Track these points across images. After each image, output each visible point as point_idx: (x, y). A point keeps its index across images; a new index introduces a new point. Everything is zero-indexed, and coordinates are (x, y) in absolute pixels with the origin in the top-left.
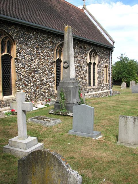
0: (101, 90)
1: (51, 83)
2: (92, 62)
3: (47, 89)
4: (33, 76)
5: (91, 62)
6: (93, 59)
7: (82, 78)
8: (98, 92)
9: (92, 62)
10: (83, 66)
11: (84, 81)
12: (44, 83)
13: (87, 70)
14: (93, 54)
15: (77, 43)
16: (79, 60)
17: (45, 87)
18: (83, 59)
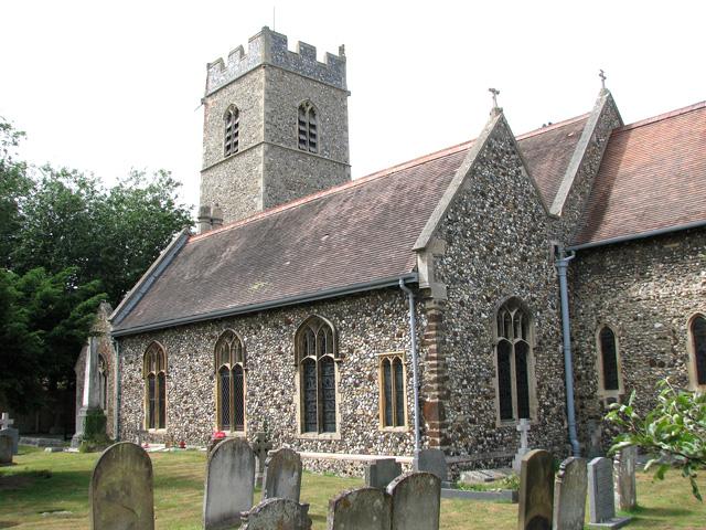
0: (361, 452)
1: (209, 414)
2: (513, 341)
4: (186, 402)
6: (516, 330)
7: (279, 407)
8: (340, 456)
9: (513, 341)
14: (513, 314)
15: (263, 318)
17: (201, 421)
18: (281, 353)
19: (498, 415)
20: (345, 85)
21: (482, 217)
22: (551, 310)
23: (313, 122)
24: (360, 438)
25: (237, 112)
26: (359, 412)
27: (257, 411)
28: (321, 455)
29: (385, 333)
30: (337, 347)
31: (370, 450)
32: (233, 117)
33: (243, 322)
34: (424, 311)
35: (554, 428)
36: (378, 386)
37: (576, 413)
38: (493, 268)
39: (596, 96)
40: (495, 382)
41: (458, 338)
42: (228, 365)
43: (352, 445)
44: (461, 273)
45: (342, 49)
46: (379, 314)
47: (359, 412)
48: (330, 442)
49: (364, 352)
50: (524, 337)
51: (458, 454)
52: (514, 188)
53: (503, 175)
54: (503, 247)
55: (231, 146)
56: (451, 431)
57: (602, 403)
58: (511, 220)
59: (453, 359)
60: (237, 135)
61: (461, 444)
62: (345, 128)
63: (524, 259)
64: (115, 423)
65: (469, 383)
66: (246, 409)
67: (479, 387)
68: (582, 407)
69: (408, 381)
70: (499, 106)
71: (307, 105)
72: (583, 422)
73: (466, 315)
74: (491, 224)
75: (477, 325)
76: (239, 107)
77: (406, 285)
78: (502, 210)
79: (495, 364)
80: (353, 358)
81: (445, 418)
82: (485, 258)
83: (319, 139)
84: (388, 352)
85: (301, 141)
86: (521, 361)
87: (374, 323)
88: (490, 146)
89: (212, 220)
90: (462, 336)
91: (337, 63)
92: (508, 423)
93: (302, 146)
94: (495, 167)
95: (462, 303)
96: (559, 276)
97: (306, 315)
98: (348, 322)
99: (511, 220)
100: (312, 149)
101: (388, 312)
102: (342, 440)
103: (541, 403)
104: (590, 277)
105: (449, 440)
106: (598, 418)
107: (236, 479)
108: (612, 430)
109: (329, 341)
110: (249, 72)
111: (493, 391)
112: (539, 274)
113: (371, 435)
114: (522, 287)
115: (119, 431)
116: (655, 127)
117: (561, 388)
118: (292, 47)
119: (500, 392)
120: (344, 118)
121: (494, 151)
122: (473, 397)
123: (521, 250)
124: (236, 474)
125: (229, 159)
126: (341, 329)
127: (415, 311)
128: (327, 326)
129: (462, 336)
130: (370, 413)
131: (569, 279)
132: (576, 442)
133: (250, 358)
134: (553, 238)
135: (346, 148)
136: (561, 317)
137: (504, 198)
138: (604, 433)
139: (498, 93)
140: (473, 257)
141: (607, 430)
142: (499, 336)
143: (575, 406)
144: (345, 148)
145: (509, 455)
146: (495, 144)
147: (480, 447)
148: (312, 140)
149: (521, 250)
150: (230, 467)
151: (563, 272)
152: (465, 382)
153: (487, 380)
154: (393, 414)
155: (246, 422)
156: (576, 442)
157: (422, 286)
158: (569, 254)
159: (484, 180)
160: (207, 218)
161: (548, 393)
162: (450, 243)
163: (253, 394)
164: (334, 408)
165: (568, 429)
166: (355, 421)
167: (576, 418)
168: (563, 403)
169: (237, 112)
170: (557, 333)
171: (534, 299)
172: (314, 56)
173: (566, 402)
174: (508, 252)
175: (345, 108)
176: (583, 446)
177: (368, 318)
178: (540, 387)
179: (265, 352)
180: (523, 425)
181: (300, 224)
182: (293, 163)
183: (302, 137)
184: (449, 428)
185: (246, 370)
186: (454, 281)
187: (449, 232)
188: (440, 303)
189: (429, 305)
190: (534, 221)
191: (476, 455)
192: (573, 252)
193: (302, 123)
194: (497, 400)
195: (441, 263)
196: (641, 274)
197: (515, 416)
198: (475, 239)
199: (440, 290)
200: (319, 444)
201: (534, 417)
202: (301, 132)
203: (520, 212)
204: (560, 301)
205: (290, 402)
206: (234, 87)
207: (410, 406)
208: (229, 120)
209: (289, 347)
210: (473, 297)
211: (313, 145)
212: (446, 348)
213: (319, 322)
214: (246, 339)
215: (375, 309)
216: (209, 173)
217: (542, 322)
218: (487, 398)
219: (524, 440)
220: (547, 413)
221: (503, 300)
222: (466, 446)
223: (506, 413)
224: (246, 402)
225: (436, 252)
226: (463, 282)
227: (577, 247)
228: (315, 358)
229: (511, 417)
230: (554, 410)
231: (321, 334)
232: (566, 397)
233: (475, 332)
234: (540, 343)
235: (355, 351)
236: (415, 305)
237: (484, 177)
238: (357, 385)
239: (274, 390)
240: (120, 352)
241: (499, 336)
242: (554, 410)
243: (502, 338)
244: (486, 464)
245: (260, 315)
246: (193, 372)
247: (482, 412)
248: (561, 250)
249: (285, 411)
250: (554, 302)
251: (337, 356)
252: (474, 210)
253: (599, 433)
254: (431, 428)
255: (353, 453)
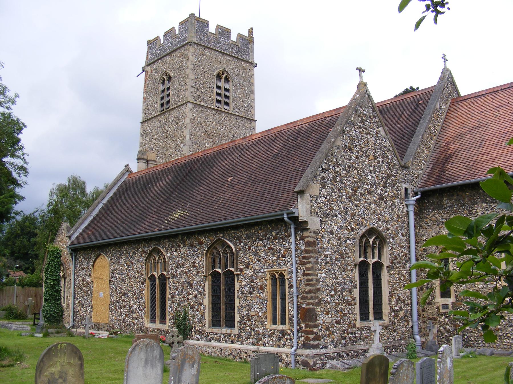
0: (253, 344)
1: (141, 310)
2: (371, 261)
3: (136, 319)
4: (123, 301)
5: (369, 261)
8: (237, 346)
9: (371, 261)
10: (195, 282)
11: (198, 313)
12: (133, 311)
13: (204, 290)
14: (371, 241)
15: (182, 239)
16: (187, 271)
17: (134, 315)
19: (358, 317)
20: (253, 58)
21: (349, 167)
22: (402, 237)
23: (227, 86)
24: (253, 333)
25: (169, 78)
26: (252, 313)
27: (176, 309)
28: (223, 345)
29: (273, 254)
30: (237, 263)
31: (260, 343)
32: (166, 82)
33: (167, 242)
34: (302, 238)
35: (401, 327)
36: (268, 289)
37: (419, 315)
38: (356, 206)
39: (438, 75)
40: (356, 293)
41: (328, 259)
42: (155, 273)
43: (247, 338)
44: (331, 209)
45: (251, 31)
46: (269, 239)
47: (252, 313)
48: (230, 335)
49: (257, 268)
50: (379, 257)
51: (326, 347)
52: (375, 144)
53: (367, 134)
54: (365, 190)
55: (165, 106)
56: (321, 330)
57: (438, 308)
58: (372, 168)
59: (324, 275)
60: (168, 95)
61: (329, 340)
62: (252, 92)
63: (381, 198)
64: (72, 314)
65: (336, 293)
66: (168, 308)
67: (343, 297)
68: (423, 311)
69: (289, 291)
70: (365, 81)
71: (223, 74)
72: (424, 322)
73: (335, 241)
74: (356, 171)
75: (343, 249)
76: (172, 75)
77: (289, 218)
78: (365, 161)
79: (357, 278)
80: (249, 272)
81: (316, 320)
82: (350, 198)
83: (231, 100)
84: (275, 268)
85: (218, 101)
86: (377, 275)
87: (265, 246)
88: (356, 112)
89: (147, 161)
90: (331, 257)
91: (247, 42)
92: (365, 324)
93: (218, 105)
94: (360, 127)
95: (332, 232)
96: (408, 212)
97: (214, 238)
98: (246, 244)
99: (372, 168)
100: (226, 107)
101: (275, 238)
102: (240, 335)
103: (391, 308)
104: (432, 212)
105: (319, 336)
106: (435, 319)
107: (149, 370)
108: (445, 328)
109: (230, 258)
110: (179, 48)
111: (354, 299)
112: (392, 210)
113: (261, 331)
114: (379, 220)
115: (74, 320)
116: (483, 99)
117: (408, 297)
118: (212, 29)
119: (360, 299)
120: (251, 84)
121: (359, 116)
122: (339, 304)
123: (379, 191)
124: (149, 365)
125: (162, 113)
126: (240, 250)
127: (295, 237)
128: (229, 247)
129: (331, 257)
130: (260, 314)
131: (416, 214)
132: (418, 337)
133: (172, 269)
134: (404, 182)
135: (252, 107)
136: (409, 243)
137: (366, 152)
138: (439, 331)
139: (364, 71)
140: (341, 197)
141: (442, 328)
142: (360, 257)
143: (418, 311)
144: (251, 107)
145: (366, 347)
146: (360, 110)
147: (344, 342)
148: (226, 100)
149: (379, 191)
150: (144, 360)
151: (411, 208)
152: (333, 293)
153: (350, 291)
154: (279, 316)
155: (168, 318)
156: (418, 337)
157: (301, 219)
158: (416, 194)
159: (352, 138)
160: (143, 159)
161: (397, 301)
162: (323, 186)
163: (173, 297)
164: (234, 310)
165: (412, 327)
166: (249, 320)
167: (419, 319)
168: (409, 308)
169: (169, 78)
170: (406, 255)
171: (388, 229)
172: (229, 37)
173: (411, 307)
174: (369, 193)
175: (252, 76)
176: (423, 339)
177: (260, 242)
178: (391, 295)
179: (183, 265)
180: (376, 326)
181: (213, 167)
182: (211, 118)
183: (219, 98)
184: (320, 328)
185: (169, 278)
186: (326, 215)
187: (323, 178)
188: (314, 233)
189: (305, 234)
190: (390, 169)
191: (341, 348)
192: (419, 193)
193: (219, 87)
194: (357, 307)
195: (316, 202)
196: (470, 211)
197: (371, 317)
198: (343, 183)
199: (314, 223)
200: (222, 336)
201: (386, 319)
202: (218, 94)
203: (378, 162)
204: (408, 230)
205: (201, 304)
206: (168, 59)
207: (291, 310)
208: (163, 83)
209: (200, 260)
210: (341, 228)
211: (227, 104)
212: (318, 266)
213: (224, 244)
214: (169, 255)
215: (266, 235)
216: (146, 124)
217: (394, 246)
218: (350, 304)
219: (376, 338)
220: (396, 316)
221: (364, 230)
222: (332, 341)
223: (364, 316)
224: (168, 303)
225: (313, 194)
226: (333, 216)
227: (421, 189)
228: (219, 270)
229: (368, 319)
230: (401, 313)
231: (225, 252)
232: (411, 303)
233: (341, 254)
234: (392, 263)
235: (250, 266)
236: (296, 234)
237: (351, 135)
238: (251, 293)
239: (189, 294)
240: (75, 260)
241: (360, 257)
242: (401, 313)
243: (362, 259)
244: (348, 355)
245: (180, 237)
246: (130, 278)
247: (345, 315)
248: (410, 191)
249: (197, 310)
250: (404, 231)
251: (237, 270)
252: (343, 161)
253: (435, 331)
254: (306, 327)
255: (248, 344)
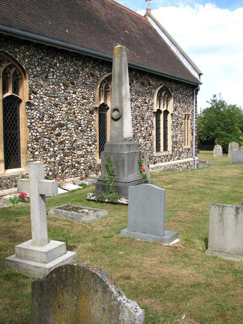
0: (178, 159)
1: (90, 145)
2: (163, 109)
3: (83, 157)
4: (59, 135)
5: (161, 109)
6: (164, 105)
7: (144, 138)
8: (172, 162)
9: (163, 109)
10: (146, 116)
11: (148, 142)
12: (78, 147)
13: (152, 124)
14: (163, 95)
15: (135, 75)
16: (140, 105)
17: (79, 153)
18: (146, 103)
